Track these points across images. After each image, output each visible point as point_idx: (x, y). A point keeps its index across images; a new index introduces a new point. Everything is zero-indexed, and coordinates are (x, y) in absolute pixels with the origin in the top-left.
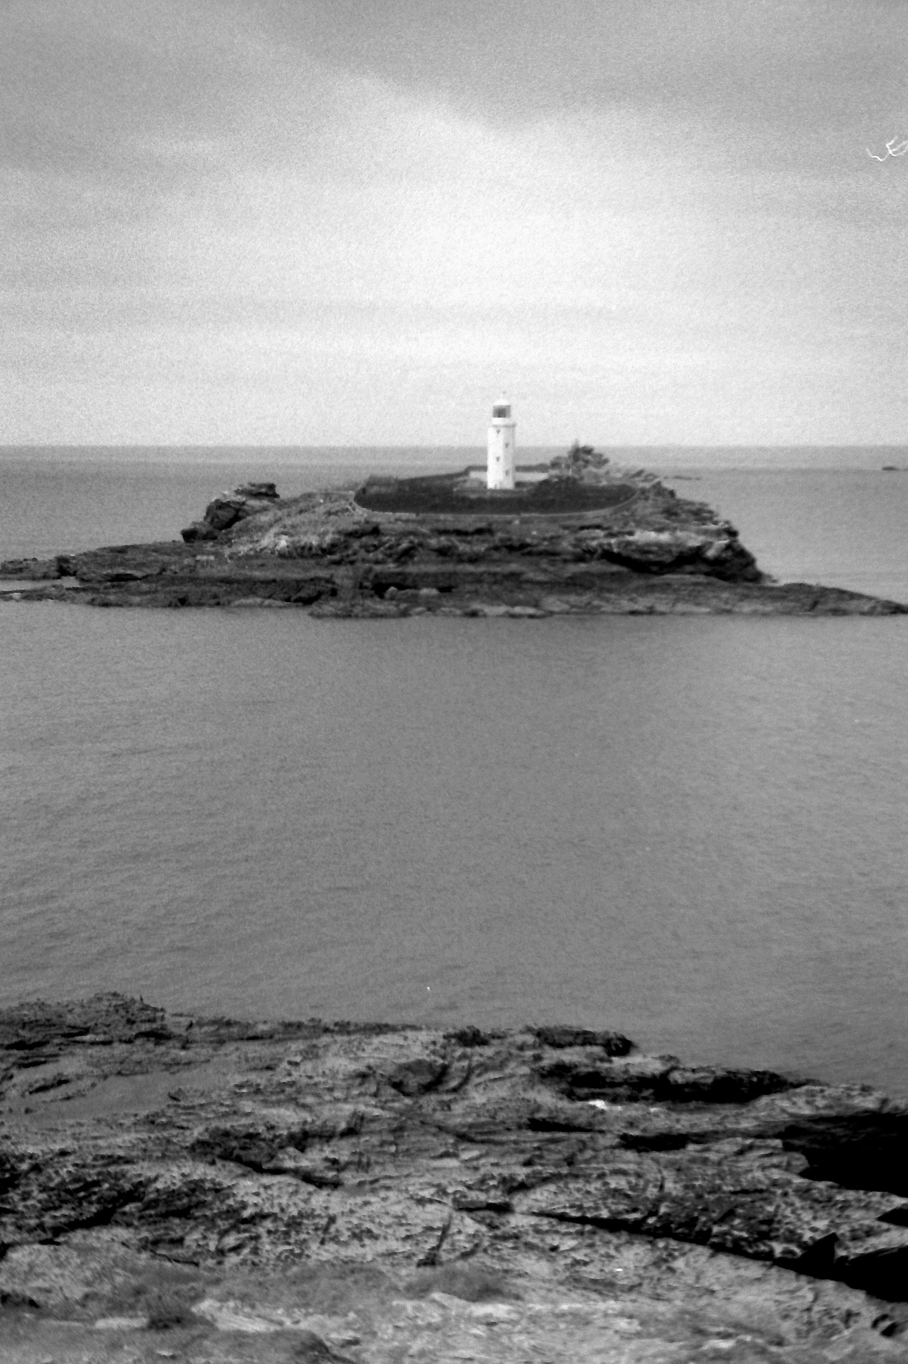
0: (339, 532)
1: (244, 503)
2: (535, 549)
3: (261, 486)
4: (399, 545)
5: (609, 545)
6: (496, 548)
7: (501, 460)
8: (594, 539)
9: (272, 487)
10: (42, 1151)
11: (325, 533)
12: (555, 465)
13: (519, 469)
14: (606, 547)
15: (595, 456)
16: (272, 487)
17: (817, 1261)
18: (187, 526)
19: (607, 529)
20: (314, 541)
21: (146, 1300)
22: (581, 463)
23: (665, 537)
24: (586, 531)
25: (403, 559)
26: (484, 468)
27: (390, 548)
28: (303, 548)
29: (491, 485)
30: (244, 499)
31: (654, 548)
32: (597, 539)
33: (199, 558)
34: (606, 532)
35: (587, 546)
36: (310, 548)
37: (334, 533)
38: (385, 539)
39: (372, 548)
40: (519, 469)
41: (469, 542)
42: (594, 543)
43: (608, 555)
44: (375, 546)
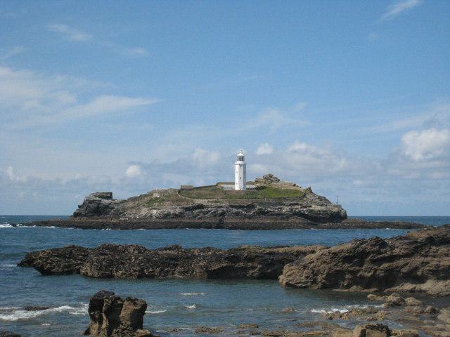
0: (183, 208)
3: (107, 193)
13: (248, 183)
15: (274, 178)
16: (111, 194)
20: (172, 212)
26: (234, 183)
27: (215, 212)
40: (248, 183)
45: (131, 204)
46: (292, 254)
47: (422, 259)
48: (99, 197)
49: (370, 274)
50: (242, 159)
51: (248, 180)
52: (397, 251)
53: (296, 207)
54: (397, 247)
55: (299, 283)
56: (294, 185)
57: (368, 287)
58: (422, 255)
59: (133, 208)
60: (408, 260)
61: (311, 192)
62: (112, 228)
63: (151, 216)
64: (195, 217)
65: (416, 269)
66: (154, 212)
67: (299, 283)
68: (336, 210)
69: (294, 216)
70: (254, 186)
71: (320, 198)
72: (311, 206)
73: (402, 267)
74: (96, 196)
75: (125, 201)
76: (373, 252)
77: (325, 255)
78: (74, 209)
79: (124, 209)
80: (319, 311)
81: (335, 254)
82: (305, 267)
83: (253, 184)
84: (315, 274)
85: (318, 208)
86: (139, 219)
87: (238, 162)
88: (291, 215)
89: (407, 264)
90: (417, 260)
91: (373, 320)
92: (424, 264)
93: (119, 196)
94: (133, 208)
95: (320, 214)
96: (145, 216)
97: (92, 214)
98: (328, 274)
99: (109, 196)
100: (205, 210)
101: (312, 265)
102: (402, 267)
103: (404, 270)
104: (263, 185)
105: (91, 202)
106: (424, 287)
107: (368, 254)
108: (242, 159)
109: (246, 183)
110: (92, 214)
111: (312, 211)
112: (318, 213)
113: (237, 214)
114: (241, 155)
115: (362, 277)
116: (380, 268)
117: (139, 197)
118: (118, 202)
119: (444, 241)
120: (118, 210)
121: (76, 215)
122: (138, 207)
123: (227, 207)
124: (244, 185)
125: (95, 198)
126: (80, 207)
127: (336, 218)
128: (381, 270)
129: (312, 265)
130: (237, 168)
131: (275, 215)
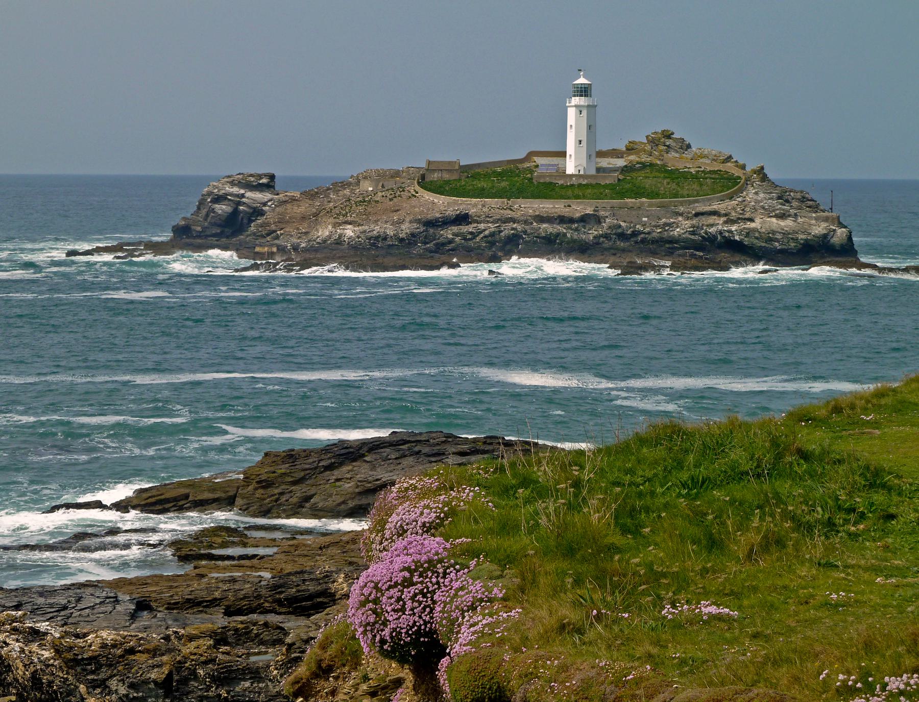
0: (419, 221)
1: (243, 196)
2: (649, 237)
3: (260, 176)
4: (501, 232)
5: (730, 231)
6: (606, 236)
7: (584, 143)
8: (712, 225)
9: (272, 177)
10: (470, 643)
11: (400, 222)
12: (631, 149)
13: (601, 154)
14: (727, 234)
15: (676, 140)
17: (284, 613)
18: (178, 221)
19: (726, 215)
23: (788, 224)
25: (508, 247)
26: (563, 154)
27: (492, 235)
28: (377, 238)
30: (242, 191)
31: (779, 236)
32: (717, 226)
34: (725, 219)
35: (706, 233)
37: (411, 222)
38: (482, 226)
39: (469, 236)
40: (601, 154)
41: (576, 230)
42: (712, 230)
44: (471, 233)
48: (240, 184)
50: (584, 91)
51: (604, 145)
53: (712, 219)
61: (764, 178)
62: (450, 439)
66: (349, 232)
70: (620, 163)
72: (751, 220)
74: (232, 184)
83: (615, 153)
87: (576, 100)
91: (347, 316)
95: (770, 240)
104: (645, 158)
108: (584, 91)
111: (755, 230)
114: (582, 81)
123: (526, 222)
124: (589, 157)
125: (229, 189)
130: (572, 113)
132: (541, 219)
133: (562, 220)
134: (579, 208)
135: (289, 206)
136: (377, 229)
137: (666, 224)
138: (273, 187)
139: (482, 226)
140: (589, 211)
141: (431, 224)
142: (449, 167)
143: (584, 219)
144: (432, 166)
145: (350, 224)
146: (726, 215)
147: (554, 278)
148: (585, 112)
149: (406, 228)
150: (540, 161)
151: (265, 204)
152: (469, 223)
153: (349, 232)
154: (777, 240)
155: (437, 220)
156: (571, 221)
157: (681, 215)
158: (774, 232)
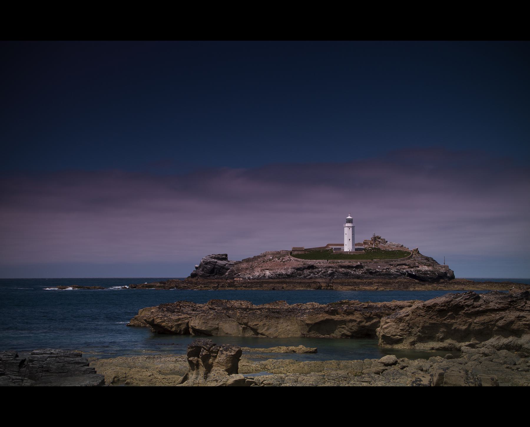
0: (294, 268)
3: (223, 255)
5: (411, 271)
6: (365, 273)
8: (404, 269)
9: (226, 255)
11: (288, 269)
13: (356, 245)
16: (226, 255)
19: (408, 265)
20: (284, 272)
21: (206, 377)
22: (377, 242)
24: (355, 264)
26: (343, 245)
27: (324, 272)
28: (279, 275)
29: (345, 250)
32: (405, 269)
33: (235, 279)
36: (282, 275)
38: (320, 269)
40: (356, 245)
41: (355, 271)
43: (410, 275)
45: (244, 265)
46: (390, 308)
47: (518, 313)
48: (215, 258)
49: (464, 328)
52: (492, 305)
54: (492, 302)
55: (395, 336)
56: (402, 246)
57: (462, 339)
58: (518, 310)
59: (247, 269)
60: (503, 313)
61: (418, 253)
63: (264, 276)
64: (305, 277)
65: (512, 322)
67: (395, 336)
68: (443, 270)
69: (401, 276)
71: (427, 259)
72: (418, 267)
73: (497, 321)
74: (212, 258)
75: (240, 262)
76: (468, 306)
77: (420, 309)
78: (192, 270)
79: (238, 270)
80: (372, 322)
81: (429, 307)
82: (401, 320)
84: (411, 326)
85: (426, 268)
86: (253, 279)
88: (399, 275)
89: (502, 318)
90: (511, 315)
92: (519, 318)
93: (233, 258)
94: (247, 269)
96: (259, 276)
97: (208, 275)
98: (423, 327)
99: (225, 258)
100: (316, 270)
101: (407, 318)
102: (497, 321)
103: (501, 323)
105: (207, 263)
106: (418, 304)
107: (462, 307)
108: (350, 221)
109: (354, 244)
110: (208, 275)
111: (420, 271)
112: (425, 273)
113: (346, 274)
114: (349, 217)
115: (457, 331)
116: (475, 321)
117: (253, 258)
118: (233, 263)
119: (527, 296)
120: (232, 271)
121: (193, 275)
122: (252, 269)
124: (353, 245)
126: (197, 268)
127: (444, 277)
128: (476, 323)
129: (407, 318)
130: (346, 230)
131: (384, 275)
132: (342, 267)
133: (349, 267)
134: (355, 263)
135: (239, 265)
136: (279, 272)
137: (387, 269)
138: (227, 259)
139: (320, 269)
140: (359, 263)
141: (298, 269)
142: (301, 250)
143: (358, 267)
144: (295, 250)
145: (268, 270)
146: (408, 265)
147: (112, 318)
148: (351, 228)
149: (290, 271)
150: (331, 247)
151: (225, 265)
152: (314, 269)
153: (268, 273)
154: (428, 274)
155: (301, 268)
156: (352, 267)
157: (392, 265)
158: (427, 271)
